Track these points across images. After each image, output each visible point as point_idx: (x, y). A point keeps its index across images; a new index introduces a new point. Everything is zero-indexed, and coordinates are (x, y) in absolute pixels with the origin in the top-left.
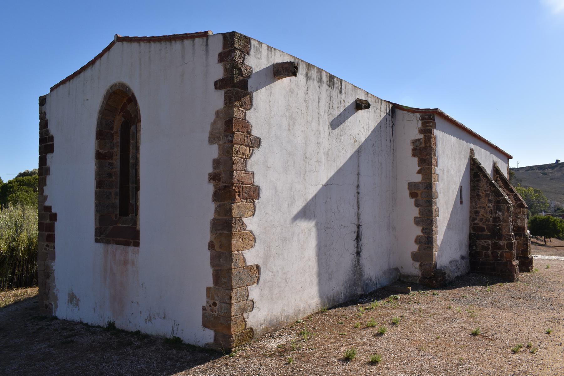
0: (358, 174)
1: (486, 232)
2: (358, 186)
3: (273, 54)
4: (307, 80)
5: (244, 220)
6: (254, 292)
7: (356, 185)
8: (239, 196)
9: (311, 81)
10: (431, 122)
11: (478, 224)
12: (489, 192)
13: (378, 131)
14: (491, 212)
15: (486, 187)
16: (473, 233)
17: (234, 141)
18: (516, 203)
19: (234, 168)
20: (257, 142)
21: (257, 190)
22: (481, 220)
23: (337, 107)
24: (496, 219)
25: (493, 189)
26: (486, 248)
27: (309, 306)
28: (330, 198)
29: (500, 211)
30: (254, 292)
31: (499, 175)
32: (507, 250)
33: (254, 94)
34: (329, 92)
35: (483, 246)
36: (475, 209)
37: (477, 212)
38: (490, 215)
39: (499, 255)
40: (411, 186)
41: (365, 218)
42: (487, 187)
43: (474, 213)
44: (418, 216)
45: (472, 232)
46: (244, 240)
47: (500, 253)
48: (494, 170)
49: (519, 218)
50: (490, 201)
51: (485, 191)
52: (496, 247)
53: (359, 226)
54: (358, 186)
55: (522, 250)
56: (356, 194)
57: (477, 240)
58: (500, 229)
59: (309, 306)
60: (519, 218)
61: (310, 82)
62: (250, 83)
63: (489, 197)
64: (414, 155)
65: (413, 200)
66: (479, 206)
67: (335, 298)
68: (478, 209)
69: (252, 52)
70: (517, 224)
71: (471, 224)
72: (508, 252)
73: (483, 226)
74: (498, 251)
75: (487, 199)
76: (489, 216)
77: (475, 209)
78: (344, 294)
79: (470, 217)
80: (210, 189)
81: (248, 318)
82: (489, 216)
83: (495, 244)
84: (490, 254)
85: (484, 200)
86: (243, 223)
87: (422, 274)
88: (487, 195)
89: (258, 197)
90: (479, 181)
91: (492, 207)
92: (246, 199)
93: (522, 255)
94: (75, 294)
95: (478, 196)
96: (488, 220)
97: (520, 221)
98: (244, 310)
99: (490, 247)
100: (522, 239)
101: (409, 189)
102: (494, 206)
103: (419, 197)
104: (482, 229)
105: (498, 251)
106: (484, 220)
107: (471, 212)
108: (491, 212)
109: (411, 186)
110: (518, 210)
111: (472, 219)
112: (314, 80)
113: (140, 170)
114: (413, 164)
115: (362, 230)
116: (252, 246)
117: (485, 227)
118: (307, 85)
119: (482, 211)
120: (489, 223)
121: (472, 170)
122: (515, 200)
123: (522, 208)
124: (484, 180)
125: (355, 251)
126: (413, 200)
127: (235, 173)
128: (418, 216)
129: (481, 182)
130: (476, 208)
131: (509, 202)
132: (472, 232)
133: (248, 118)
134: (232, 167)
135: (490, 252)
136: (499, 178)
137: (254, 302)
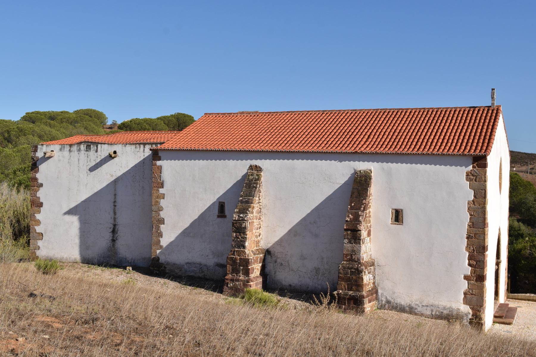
0: (115, 195)
2: (115, 202)
3: (49, 147)
4: (70, 153)
5: (35, 215)
6: (40, 243)
7: (113, 201)
9: (73, 152)
20: (41, 185)
21: (42, 204)
27: (70, 258)
28: (88, 208)
30: (40, 243)
33: (39, 167)
34: (86, 155)
41: (122, 220)
53: (115, 225)
54: (115, 202)
56: (113, 207)
59: (70, 258)
61: (72, 153)
62: (38, 163)
67: (89, 260)
69: (38, 151)
78: (97, 260)
80: (76, 110)
89: (42, 206)
112: (74, 151)
113: (500, 272)
115: (118, 228)
116: (39, 225)
125: (111, 238)
133: (37, 177)
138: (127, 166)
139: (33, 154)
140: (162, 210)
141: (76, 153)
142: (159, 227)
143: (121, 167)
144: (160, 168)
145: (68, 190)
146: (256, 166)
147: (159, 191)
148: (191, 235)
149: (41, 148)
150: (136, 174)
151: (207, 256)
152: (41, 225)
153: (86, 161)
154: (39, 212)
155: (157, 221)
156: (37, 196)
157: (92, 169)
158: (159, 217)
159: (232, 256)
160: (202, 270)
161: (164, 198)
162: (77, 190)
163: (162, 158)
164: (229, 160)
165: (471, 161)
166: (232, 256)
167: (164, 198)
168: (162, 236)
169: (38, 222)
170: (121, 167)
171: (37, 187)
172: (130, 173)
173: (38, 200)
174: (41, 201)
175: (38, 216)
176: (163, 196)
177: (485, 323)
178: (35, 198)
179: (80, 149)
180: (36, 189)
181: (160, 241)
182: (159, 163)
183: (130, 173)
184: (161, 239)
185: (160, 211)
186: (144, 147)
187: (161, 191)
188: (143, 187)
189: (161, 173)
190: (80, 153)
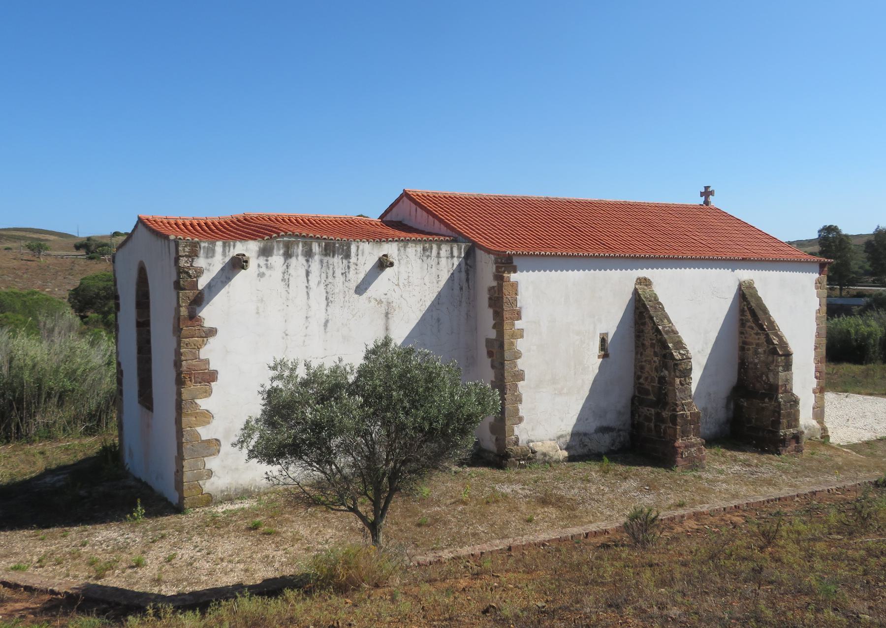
1: (652, 397)
4: (286, 259)
8: (191, 381)
10: (502, 267)
11: (643, 384)
12: (654, 342)
13: (433, 282)
14: (656, 370)
15: (651, 334)
16: (638, 397)
17: (181, 337)
18: (768, 347)
19: (183, 358)
22: (646, 379)
23: (342, 274)
24: (662, 380)
25: (659, 337)
26: (648, 419)
29: (666, 369)
30: (212, 463)
31: (747, 302)
32: (671, 425)
35: (645, 415)
36: (640, 364)
37: (642, 368)
38: (656, 374)
39: (662, 430)
40: (489, 342)
42: (653, 334)
43: (639, 369)
44: (494, 380)
45: (637, 394)
46: (198, 418)
47: (663, 427)
48: (740, 294)
49: (772, 371)
50: (656, 354)
51: (651, 339)
52: (659, 419)
55: (773, 420)
57: (640, 407)
58: (666, 394)
60: (772, 371)
61: (293, 261)
63: (654, 348)
64: (490, 306)
65: (490, 360)
66: (644, 359)
68: (643, 363)
70: (769, 380)
71: (635, 384)
72: (671, 427)
73: (647, 387)
74: (661, 425)
75: (653, 350)
76: (654, 374)
77: (640, 364)
79: (635, 373)
81: (204, 485)
82: (654, 374)
83: (658, 415)
84: (653, 427)
85: (649, 352)
86: (196, 403)
87: (498, 450)
88: (653, 345)
90: (644, 324)
91: (657, 361)
92: (200, 383)
93: (772, 428)
94: (241, 432)
95: (643, 345)
96: (653, 380)
97: (772, 375)
98: (200, 477)
99: (653, 418)
100: (773, 403)
101: (487, 346)
102: (660, 361)
103: (495, 358)
104: (647, 392)
105: (661, 425)
106: (649, 380)
107: (635, 366)
108: (656, 370)
109: (489, 342)
110: (770, 358)
111: (638, 378)
112: (297, 256)
114: (487, 316)
116: (209, 423)
117: (650, 388)
118: (286, 264)
119: (647, 367)
120: (654, 384)
121: (637, 308)
122: (767, 343)
123: (775, 356)
124: (649, 324)
126: (490, 360)
127: (184, 363)
128: (494, 380)
129: (647, 326)
130: (642, 362)
131: (774, 341)
132: (637, 394)
134: (180, 358)
135: (652, 425)
136: (746, 307)
137: (213, 471)
138: (409, 282)
139: (186, 262)
140: (520, 357)
141: (302, 259)
142: (517, 385)
143: (398, 285)
144: (515, 286)
145: (283, 338)
146: (645, 279)
147: (514, 325)
148: (565, 391)
149: (208, 248)
150: (425, 296)
151: (587, 419)
152: (214, 423)
153: (324, 276)
154: (208, 393)
155: (512, 377)
156: (202, 356)
157: (361, 289)
158: (516, 369)
159: (682, 412)
160: (583, 443)
161: (522, 337)
162: (305, 336)
163: (518, 268)
164: (637, 269)
165: (817, 267)
166: (682, 412)
167: (522, 337)
168: (520, 401)
169: (206, 417)
170: (398, 285)
171: (201, 337)
172: (414, 295)
173: (204, 368)
174: (212, 367)
175: (203, 404)
176: (520, 334)
177: (559, 438)
178: (194, 362)
179: (311, 250)
180: (197, 341)
181: (518, 410)
182: (514, 277)
183: (414, 295)
184: (520, 407)
185: (517, 358)
186: (439, 249)
187: (518, 324)
188: (439, 320)
189: (516, 294)
190: (310, 260)
